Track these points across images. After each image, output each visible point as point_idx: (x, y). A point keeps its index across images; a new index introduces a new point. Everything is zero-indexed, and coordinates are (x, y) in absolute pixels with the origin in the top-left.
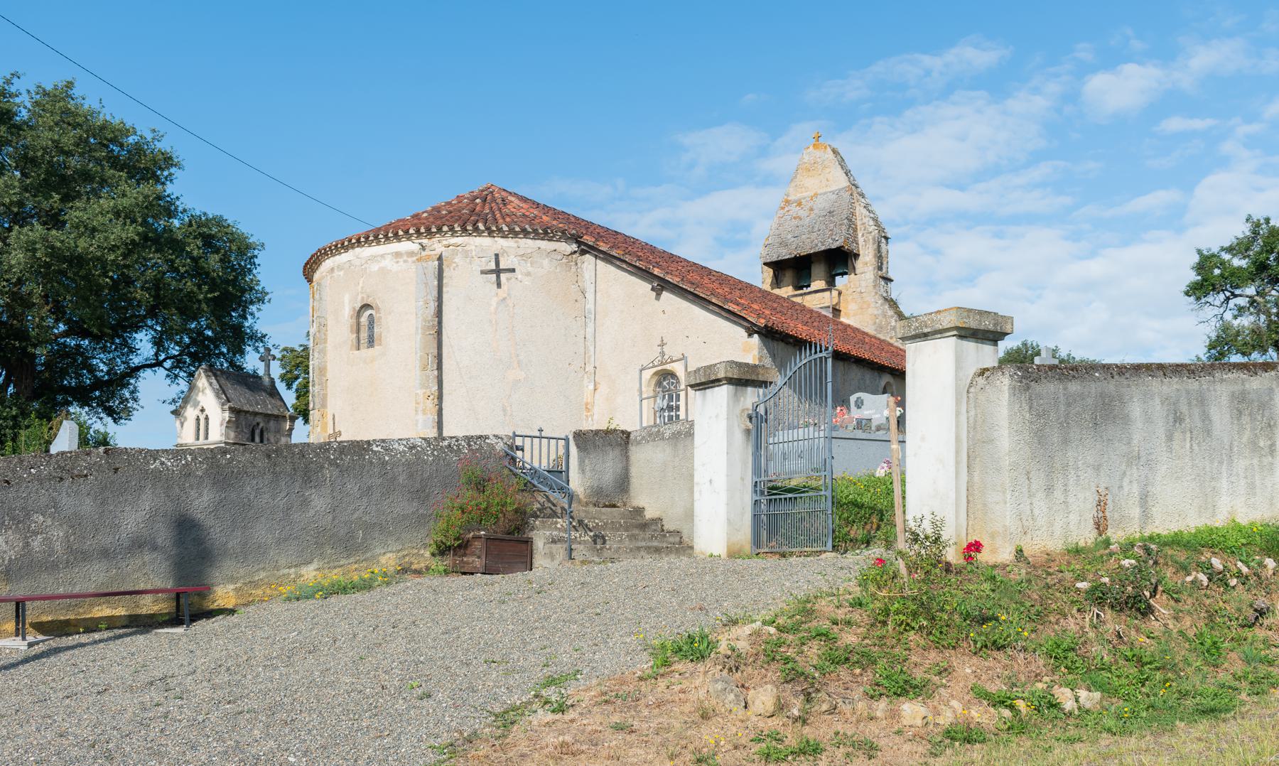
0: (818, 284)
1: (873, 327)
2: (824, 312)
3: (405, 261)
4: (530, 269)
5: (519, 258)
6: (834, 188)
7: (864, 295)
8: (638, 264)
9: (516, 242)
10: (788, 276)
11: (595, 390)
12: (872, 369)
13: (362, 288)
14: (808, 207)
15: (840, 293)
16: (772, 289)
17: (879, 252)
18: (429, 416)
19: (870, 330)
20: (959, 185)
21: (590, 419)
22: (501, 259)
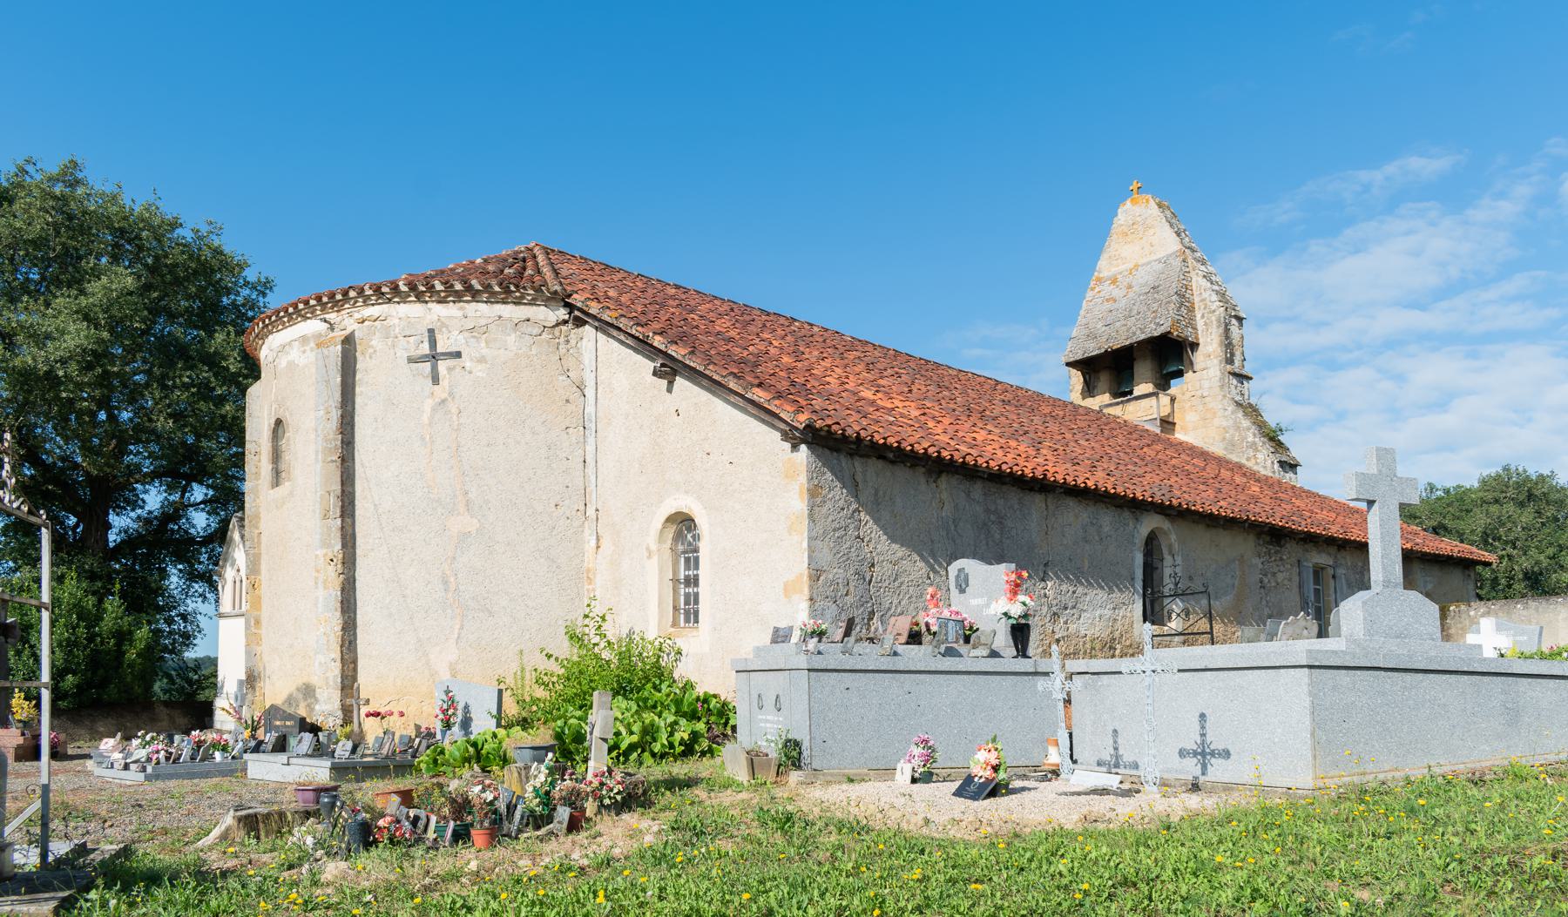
0: (1141, 389)
1: (1222, 445)
2: (1148, 427)
4: (485, 351)
5: (467, 334)
6: (1161, 254)
7: (1207, 399)
8: (634, 332)
9: (461, 308)
10: (1104, 379)
11: (598, 547)
12: (1116, 506)
14: (1125, 283)
15: (1173, 400)
16: (1084, 399)
17: (1227, 337)
19: (1217, 449)
20: (1417, 303)
22: (438, 337)
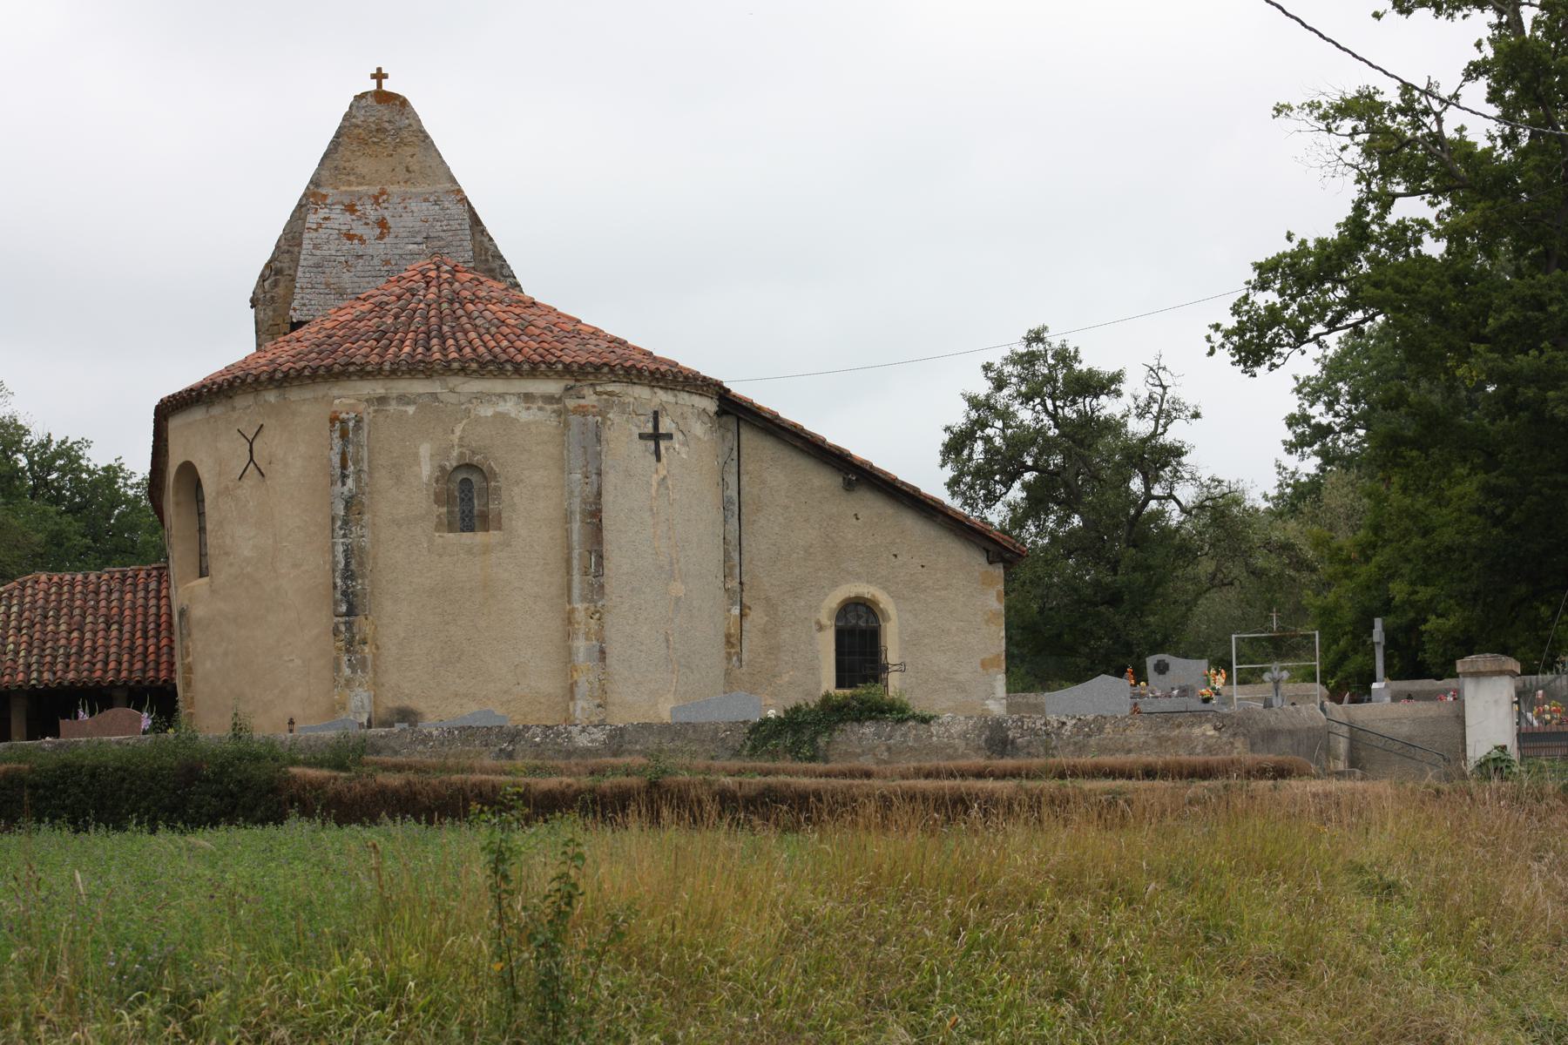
3: (540, 409)
13: (461, 438)
18: (594, 642)
21: (735, 658)
